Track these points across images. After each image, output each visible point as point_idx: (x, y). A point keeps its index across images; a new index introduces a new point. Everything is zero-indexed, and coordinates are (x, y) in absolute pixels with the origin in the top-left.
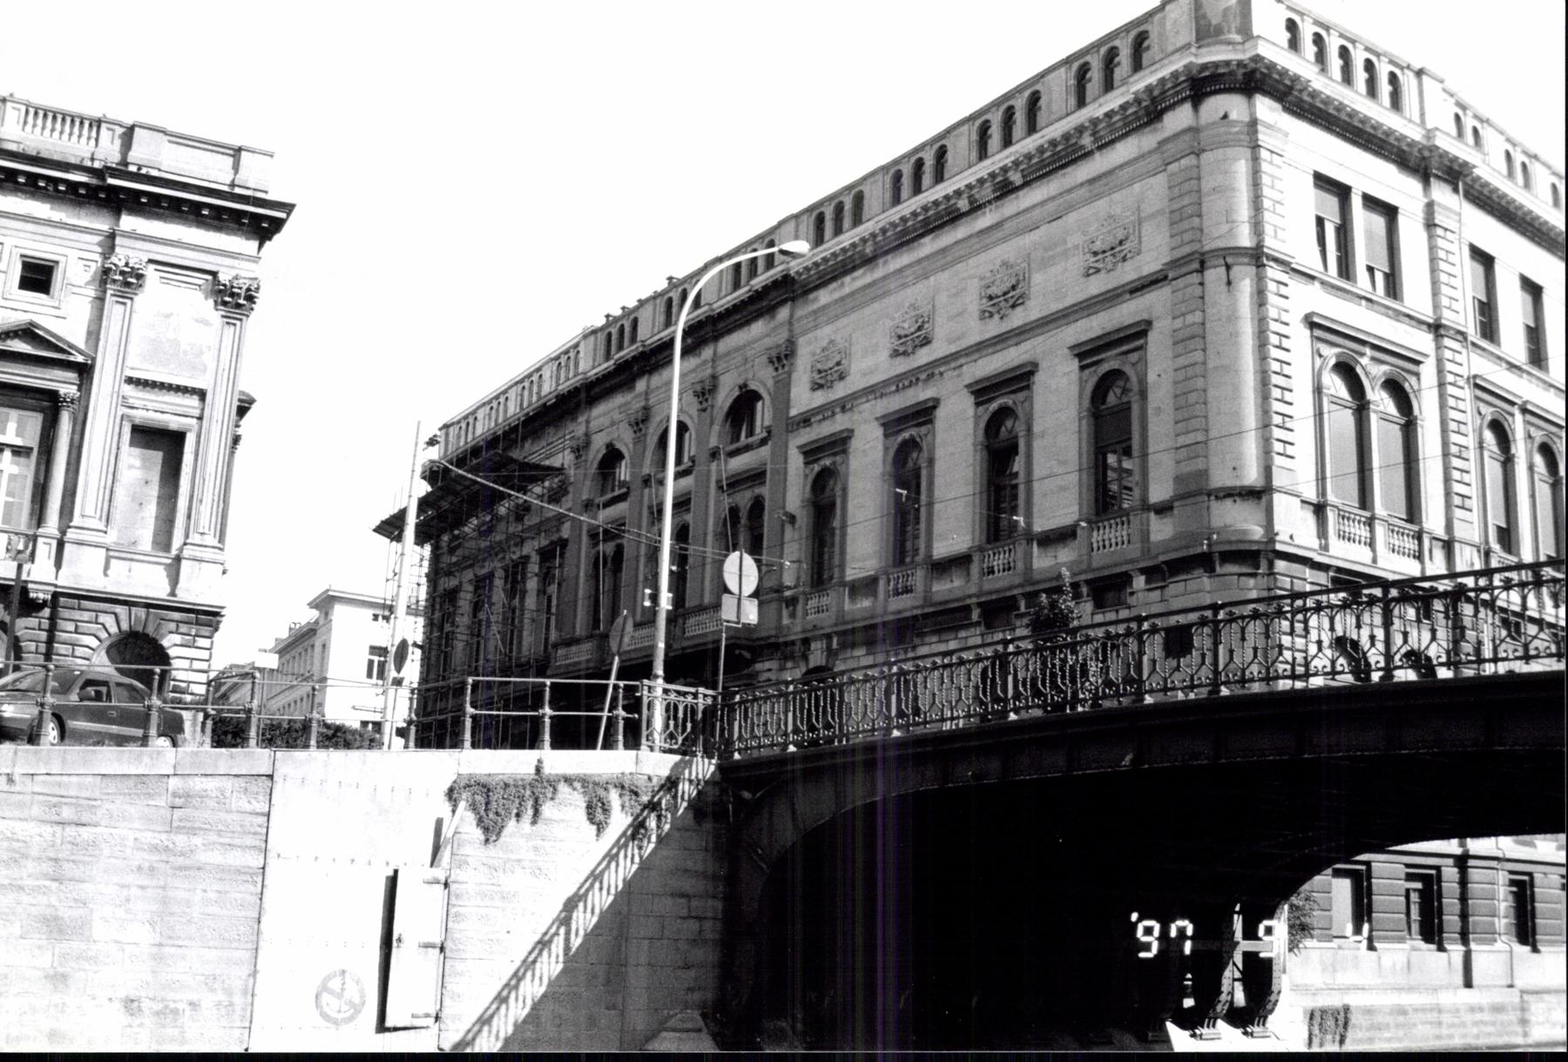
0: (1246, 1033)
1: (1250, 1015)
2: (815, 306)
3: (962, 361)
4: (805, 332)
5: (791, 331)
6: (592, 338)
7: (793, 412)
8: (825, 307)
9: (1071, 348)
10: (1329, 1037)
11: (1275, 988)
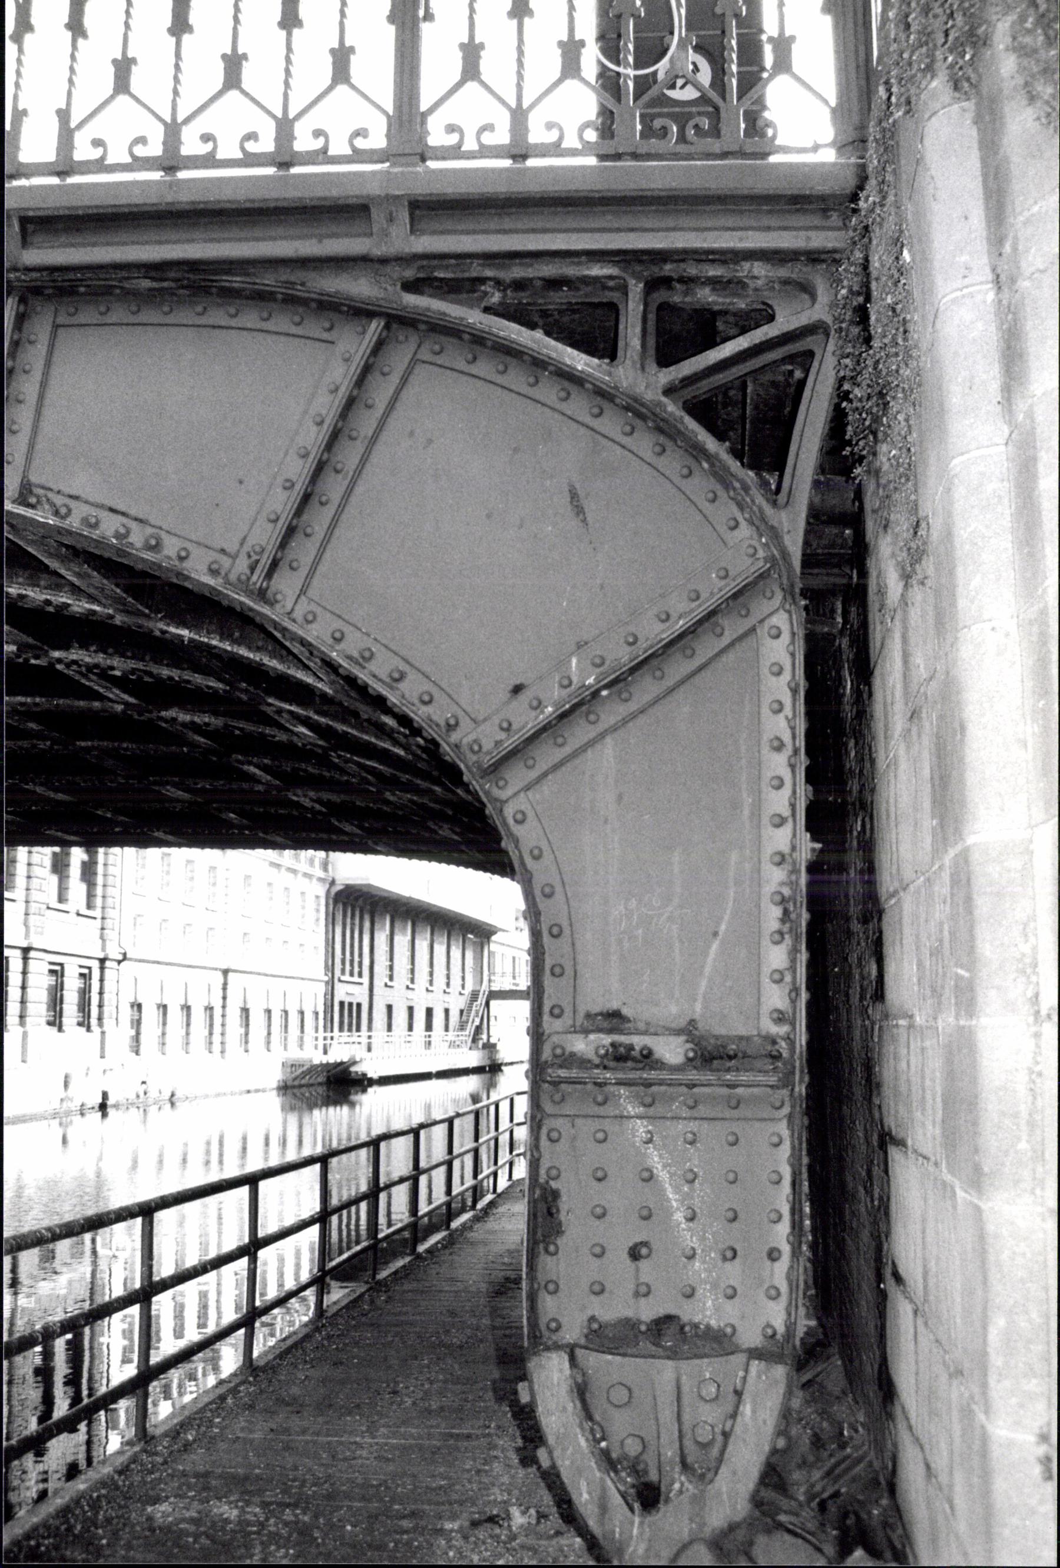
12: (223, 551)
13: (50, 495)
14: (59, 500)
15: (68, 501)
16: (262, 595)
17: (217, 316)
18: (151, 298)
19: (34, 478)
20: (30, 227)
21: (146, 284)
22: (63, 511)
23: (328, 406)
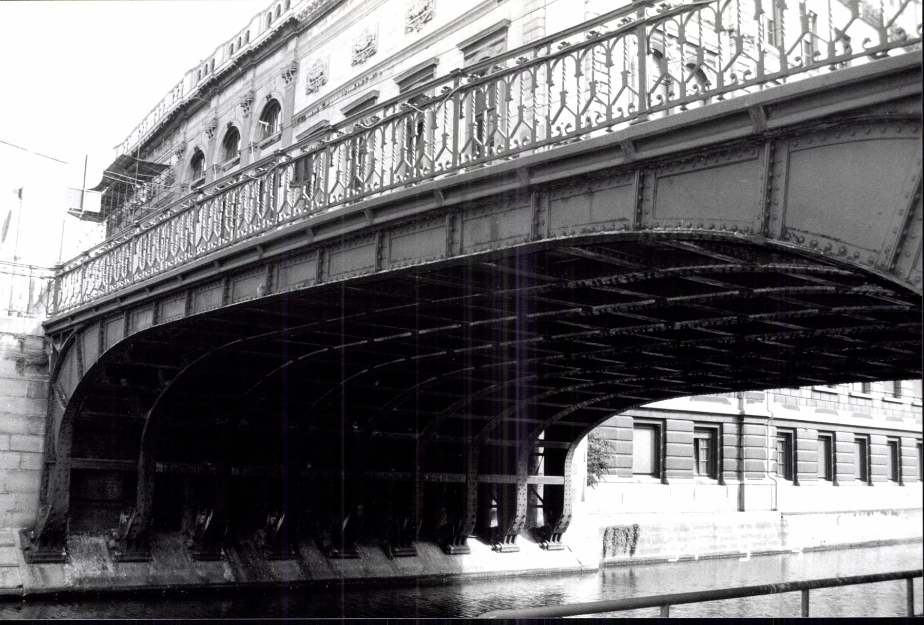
0: (542, 547)
1: (547, 533)
2: (309, 38)
3: (394, 62)
4: (305, 55)
5: (296, 56)
6: (190, 75)
7: (296, 112)
8: (315, 38)
9: (458, 45)
10: (621, 549)
11: (566, 512)
12: (874, 251)
13: (795, 232)
14: (799, 234)
15: (802, 234)
16: (893, 271)
17: (860, 135)
18: (829, 132)
19: (788, 225)
20: (770, 109)
21: (825, 126)
22: (801, 239)
23: (761, 184)
